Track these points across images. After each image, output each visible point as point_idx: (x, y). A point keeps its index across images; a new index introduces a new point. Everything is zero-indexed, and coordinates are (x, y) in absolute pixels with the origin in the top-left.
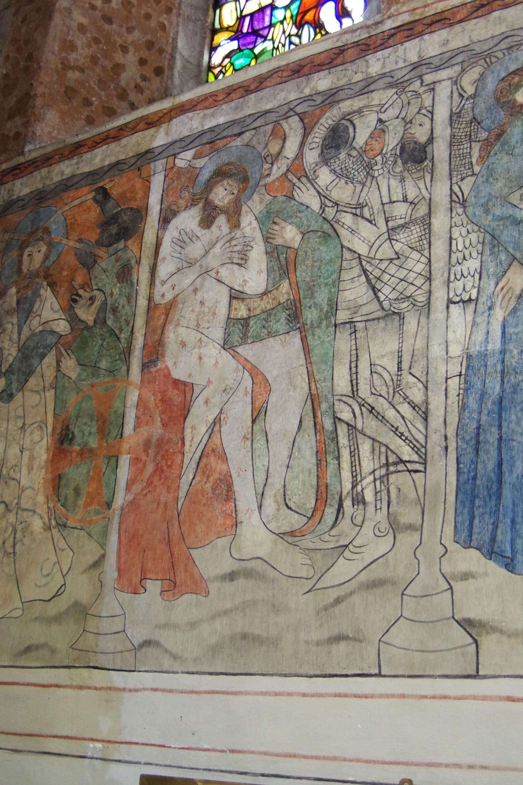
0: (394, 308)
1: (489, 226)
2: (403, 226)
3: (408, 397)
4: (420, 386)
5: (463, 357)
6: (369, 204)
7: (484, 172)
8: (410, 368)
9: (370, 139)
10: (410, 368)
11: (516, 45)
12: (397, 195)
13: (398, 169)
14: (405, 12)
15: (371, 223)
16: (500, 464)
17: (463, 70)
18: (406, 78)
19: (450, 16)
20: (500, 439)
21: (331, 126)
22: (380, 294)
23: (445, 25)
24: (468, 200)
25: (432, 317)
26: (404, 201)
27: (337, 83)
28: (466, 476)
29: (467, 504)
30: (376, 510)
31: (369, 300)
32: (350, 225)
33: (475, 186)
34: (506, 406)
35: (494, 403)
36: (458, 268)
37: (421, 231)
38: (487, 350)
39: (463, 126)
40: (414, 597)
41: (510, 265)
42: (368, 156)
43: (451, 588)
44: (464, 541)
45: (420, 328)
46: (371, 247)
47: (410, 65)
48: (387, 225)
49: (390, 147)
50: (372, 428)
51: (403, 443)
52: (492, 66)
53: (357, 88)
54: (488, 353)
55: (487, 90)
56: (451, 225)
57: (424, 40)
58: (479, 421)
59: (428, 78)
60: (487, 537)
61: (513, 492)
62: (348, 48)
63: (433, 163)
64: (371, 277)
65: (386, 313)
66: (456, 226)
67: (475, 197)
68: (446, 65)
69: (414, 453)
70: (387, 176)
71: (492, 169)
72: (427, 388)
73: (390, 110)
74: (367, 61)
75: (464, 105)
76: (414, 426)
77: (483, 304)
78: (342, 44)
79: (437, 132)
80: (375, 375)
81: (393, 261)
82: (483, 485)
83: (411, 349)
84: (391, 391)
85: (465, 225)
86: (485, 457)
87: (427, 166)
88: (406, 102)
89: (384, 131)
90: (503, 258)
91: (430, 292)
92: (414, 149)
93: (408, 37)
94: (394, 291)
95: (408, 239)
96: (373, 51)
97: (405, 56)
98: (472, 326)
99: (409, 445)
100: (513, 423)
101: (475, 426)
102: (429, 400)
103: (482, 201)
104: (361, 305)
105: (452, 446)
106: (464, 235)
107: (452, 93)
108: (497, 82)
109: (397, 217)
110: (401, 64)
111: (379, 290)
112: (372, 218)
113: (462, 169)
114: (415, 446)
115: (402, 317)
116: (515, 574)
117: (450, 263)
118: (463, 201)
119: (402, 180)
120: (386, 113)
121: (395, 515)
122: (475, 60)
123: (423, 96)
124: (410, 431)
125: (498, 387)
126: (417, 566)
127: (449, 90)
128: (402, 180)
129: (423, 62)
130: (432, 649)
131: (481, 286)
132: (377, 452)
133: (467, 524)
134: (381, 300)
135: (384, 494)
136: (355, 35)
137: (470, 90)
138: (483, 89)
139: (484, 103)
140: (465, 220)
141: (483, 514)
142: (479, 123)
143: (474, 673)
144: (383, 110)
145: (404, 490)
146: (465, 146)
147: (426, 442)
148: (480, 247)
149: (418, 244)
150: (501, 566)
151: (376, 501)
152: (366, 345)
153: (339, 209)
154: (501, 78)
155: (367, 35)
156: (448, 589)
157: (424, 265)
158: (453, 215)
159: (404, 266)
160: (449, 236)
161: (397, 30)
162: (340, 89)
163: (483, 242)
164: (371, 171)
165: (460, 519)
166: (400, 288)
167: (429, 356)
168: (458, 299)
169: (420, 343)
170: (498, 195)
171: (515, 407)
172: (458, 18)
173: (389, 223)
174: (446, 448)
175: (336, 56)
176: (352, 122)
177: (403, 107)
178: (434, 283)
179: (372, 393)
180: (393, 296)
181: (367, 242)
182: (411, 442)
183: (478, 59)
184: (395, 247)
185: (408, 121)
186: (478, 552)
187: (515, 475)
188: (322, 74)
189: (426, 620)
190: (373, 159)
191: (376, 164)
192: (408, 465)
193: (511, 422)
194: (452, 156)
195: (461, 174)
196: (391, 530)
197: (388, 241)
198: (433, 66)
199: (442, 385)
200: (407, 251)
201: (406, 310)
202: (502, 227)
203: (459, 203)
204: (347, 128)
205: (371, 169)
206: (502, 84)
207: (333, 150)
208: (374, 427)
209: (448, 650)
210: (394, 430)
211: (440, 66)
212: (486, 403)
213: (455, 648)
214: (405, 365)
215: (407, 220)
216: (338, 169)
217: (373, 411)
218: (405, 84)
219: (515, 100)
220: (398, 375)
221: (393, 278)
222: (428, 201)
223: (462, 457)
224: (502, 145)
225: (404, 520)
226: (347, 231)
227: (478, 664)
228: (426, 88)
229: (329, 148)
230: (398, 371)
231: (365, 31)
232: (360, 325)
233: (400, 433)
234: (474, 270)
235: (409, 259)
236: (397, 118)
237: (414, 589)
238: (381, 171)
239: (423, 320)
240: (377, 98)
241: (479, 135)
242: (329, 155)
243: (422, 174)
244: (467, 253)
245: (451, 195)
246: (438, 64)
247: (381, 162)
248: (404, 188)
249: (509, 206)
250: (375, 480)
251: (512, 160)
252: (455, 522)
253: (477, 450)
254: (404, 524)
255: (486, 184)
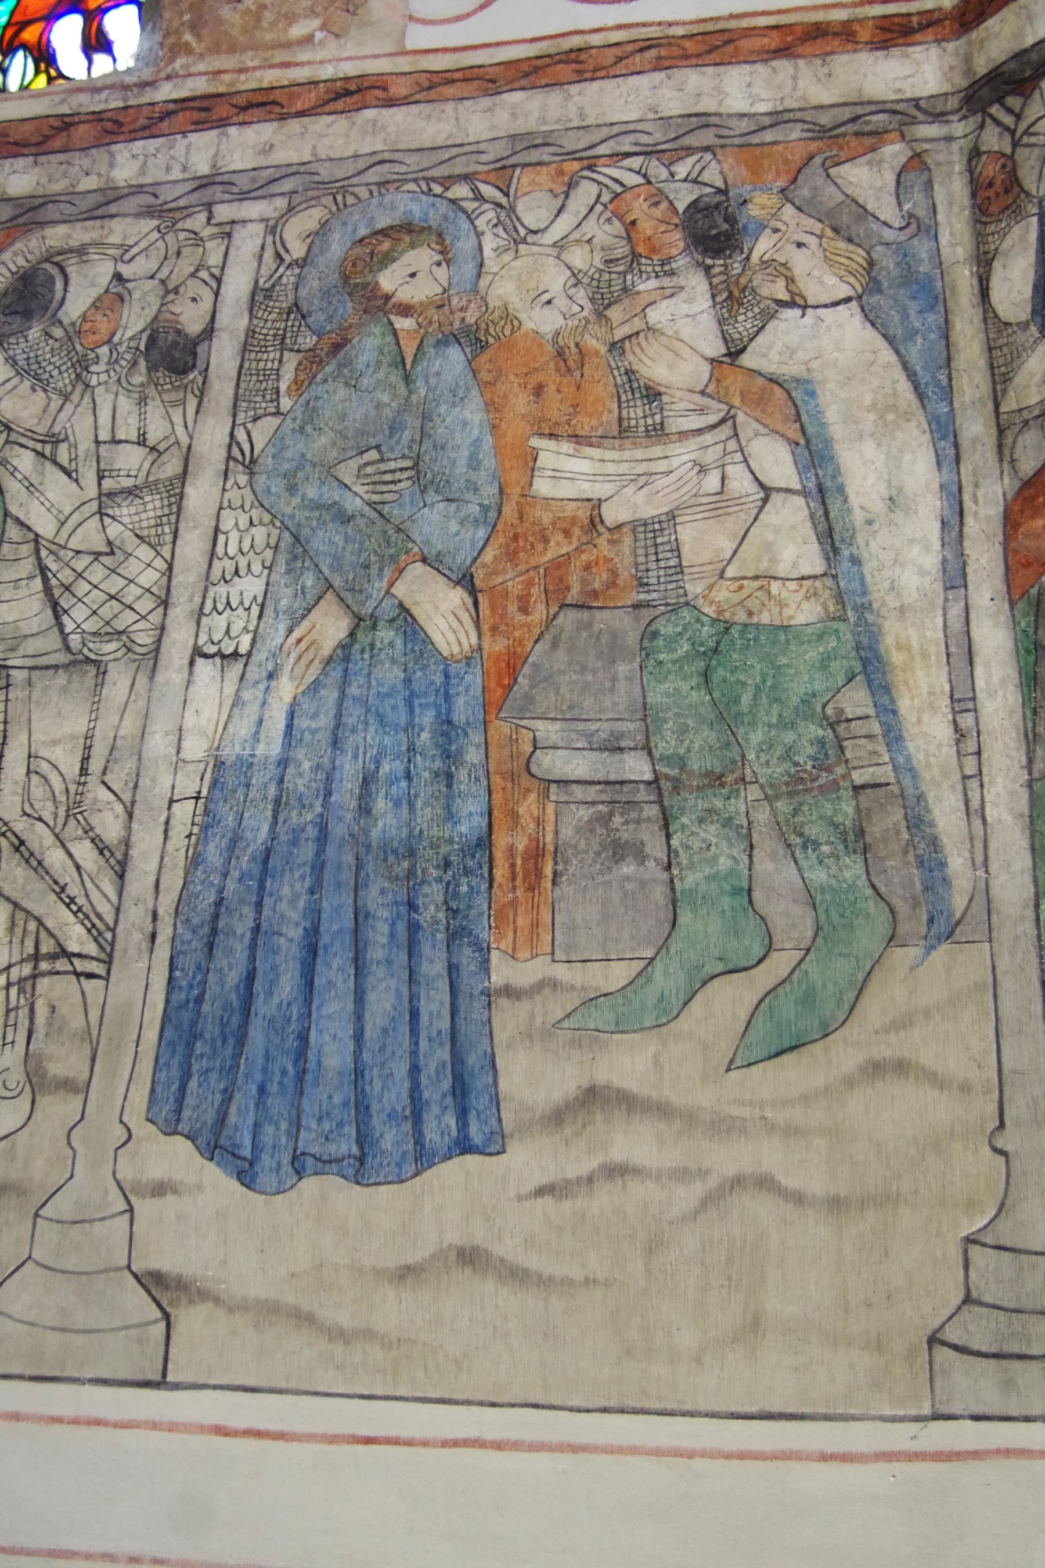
0: (90, 650)
1: (292, 517)
2: (130, 492)
3: (92, 829)
4: (119, 809)
5: (207, 764)
6: (71, 439)
7: (298, 413)
8: (104, 773)
9: (93, 311)
10: (104, 773)
11: (395, 181)
12: (127, 430)
13: (138, 379)
14: (200, 74)
15: (70, 476)
16: (251, 977)
17: (291, 209)
18: (181, 203)
19: (284, 100)
20: (257, 929)
21: (22, 270)
22: (65, 619)
23: (273, 116)
24: (260, 461)
25: (160, 677)
26: (139, 444)
27: (47, 186)
28: (183, 996)
29: (180, 1049)
30: (4, 1045)
31: (44, 627)
32: (27, 475)
33: (276, 437)
34: (275, 868)
35: (253, 859)
36: (222, 590)
37: (162, 507)
38: (253, 756)
39: (274, 316)
40: (58, 1222)
41: (320, 598)
42: (84, 342)
43: (131, 1210)
44: (166, 1120)
45: (133, 697)
46: (63, 524)
47: (194, 179)
48: (100, 485)
49: (129, 333)
50: (15, 881)
51: (71, 918)
52: (345, 212)
53: (84, 204)
54: (256, 761)
55: (329, 255)
56: (221, 503)
57: (228, 136)
58: (221, 891)
59: (223, 212)
60: (210, 1117)
61: (267, 1036)
62: (80, 122)
63: (205, 377)
64: (54, 582)
65: (70, 657)
66: (230, 507)
67: (274, 457)
68: (260, 193)
69: (91, 939)
70: (114, 389)
71: (315, 409)
72: (130, 815)
73: (141, 260)
74: (112, 155)
75: (281, 276)
76: (97, 887)
77: (260, 666)
78: (69, 112)
79: (224, 318)
80: (35, 778)
81: (101, 558)
82: (214, 1017)
83: (112, 734)
84: (62, 813)
85: (247, 508)
86: (225, 962)
87: (193, 381)
88: (173, 250)
89: (122, 300)
90: (309, 583)
91: (163, 628)
92: (175, 344)
93: (197, 123)
94: (95, 617)
95: (136, 518)
96: (127, 136)
97: (187, 159)
98: (233, 705)
99: (83, 924)
100: (285, 901)
101: (212, 899)
102: (133, 839)
103: (286, 466)
104: (26, 636)
105: (165, 933)
106: (242, 528)
107: (263, 248)
108: (349, 244)
109: (122, 473)
110: (176, 174)
111: (66, 612)
112: (73, 466)
113: (259, 399)
114: (94, 926)
115: (102, 670)
116: (254, 1191)
117: (207, 578)
118: (251, 461)
119: (142, 401)
120: (132, 264)
121: (40, 1057)
122: (317, 193)
123: (208, 245)
124: (87, 896)
125: (265, 829)
126: (70, 1162)
127: (259, 242)
128: (142, 401)
129: (219, 179)
130: (81, 1327)
131: (260, 630)
132: (19, 930)
133: (175, 1087)
134: (67, 630)
135: (23, 1014)
136: (97, 97)
137: (297, 250)
138: (322, 252)
139: (320, 279)
140: (249, 498)
141: (207, 1071)
142: (304, 317)
143: (157, 1377)
144: (127, 257)
145: (63, 1009)
146: (272, 356)
147: (116, 921)
148: (269, 554)
149: (153, 531)
150: (231, 1175)
151: (6, 1026)
152: (25, 717)
153: (11, 439)
154: (359, 237)
155: (120, 104)
156: (125, 1211)
157: (158, 575)
158: (228, 486)
159: (120, 570)
160: (213, 524)
161: (179, 106)
162: (51, 200)
163: (276, 547)
164: (85, 373)
165: (163, 1076)
166: (106, 612)
167: (144, 754)
168: (212, 649)
169: (129, 726)
170: (316, 460)
171: (291, 870)
172: (299, 106)
173: (103, 482)
174: (153, 936)
175: (53, 132)
176: (62, 270)
177: (166, 258)
178: (172, 612)
179: (25, 814)
180: (90, 626)
181: (55, 512)
182: (87, 917)
183: (321, 192)
184: (108, 530)
185: (171, 287)
186: (189, 1143)
187: (276, 1001)
188: (20, 163)
189: (77, 1270)
190: (92, 350)
191: (97, 360)
192: (76, 961)
193: (281, 900)
194: (244, 371)
195: (255, 409)
196: (28, 1088)
197: (97, 516)
198: (236, 190)
199: (160, 813)
200: (131, 542)
201: (111, 657)
202: (315, 523)
203: (243, 464)
204: (52, 279)
205: (86, 369)
206: (358, 250)
207: (18, 319)
208: (21, 881)
209: (113, 1330)
210: (58, 890)
211: (249, 192)
212: (238, 858)
213: (126, 1328)
214: (96, 765)
215: (139, 481)
216: (21, 358)
217: (22, 848)
218: (178, 215)
219: (377, 283)
220: (79, 784)
221: (95, 591)
222: (184, 450)
223: (181, 957)
224: (340, 366)
225: (55, 1069)
226: (19, 485)
227: (166, 1360)
228: (216, 230)
229: (10, 314)
230: (81, 775)
231: (118, 94)
232: (18, 676)
233: (68, 897)
234: (251, 598)
235: (132, 558)
236: (152, 277)
237: (62, 1206)
238: (103, 377)
239: (142, 681)
240: (119, 231)
241: (300, 340)
242: (7, 328)
243: (181, 395)
244: (243, 563)
245: (230, 446)
246: (245, 188)
247: (106, 359)
248: (142, 417)
249: (335, 484)
250: (9, 985)
251: (354, 397)
252: (153, 1082)
253: (211, 946)
254: (54, 1077)
255: (298, 435)
